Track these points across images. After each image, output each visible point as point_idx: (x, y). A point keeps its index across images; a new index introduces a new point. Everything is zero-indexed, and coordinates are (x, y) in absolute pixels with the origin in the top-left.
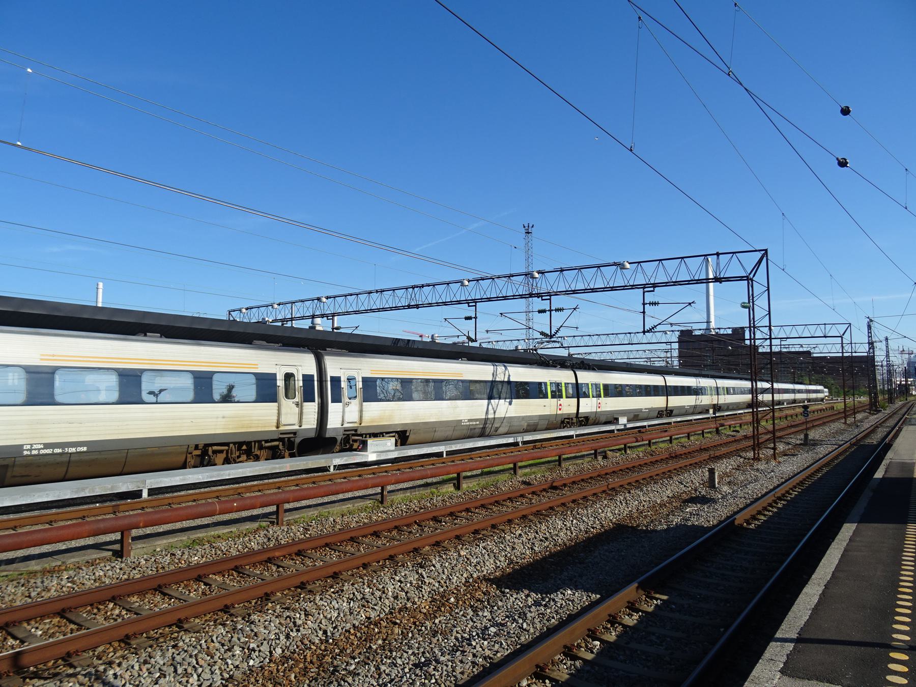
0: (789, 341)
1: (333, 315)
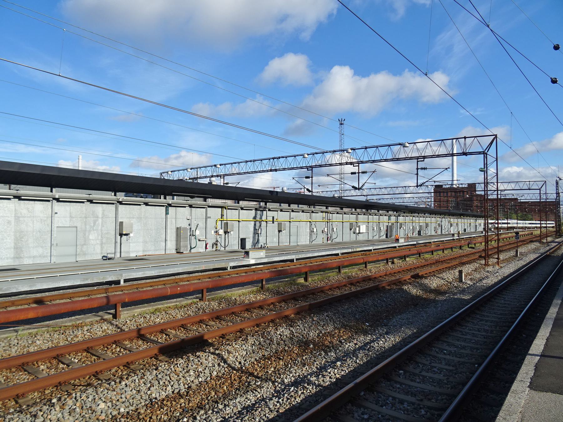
0: (506, 192)
1: (224, 175)
